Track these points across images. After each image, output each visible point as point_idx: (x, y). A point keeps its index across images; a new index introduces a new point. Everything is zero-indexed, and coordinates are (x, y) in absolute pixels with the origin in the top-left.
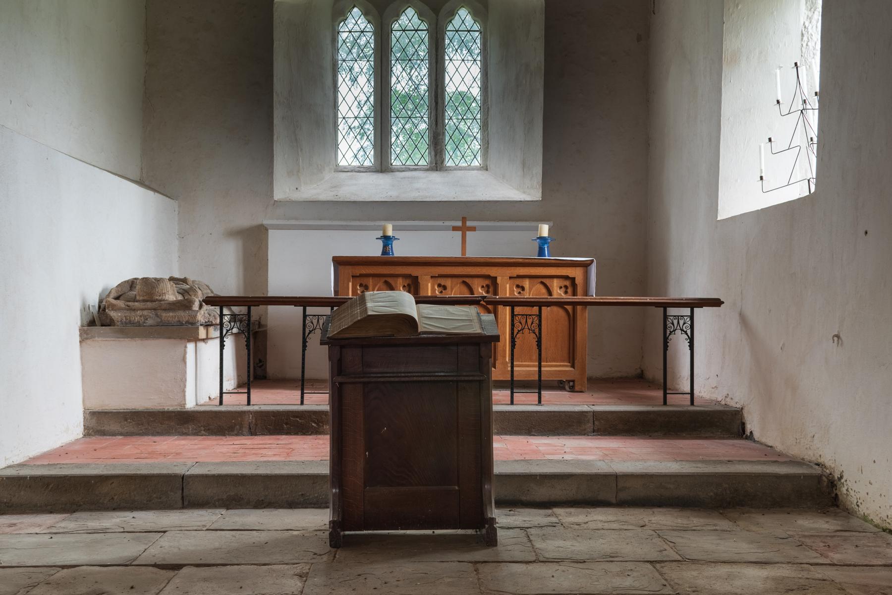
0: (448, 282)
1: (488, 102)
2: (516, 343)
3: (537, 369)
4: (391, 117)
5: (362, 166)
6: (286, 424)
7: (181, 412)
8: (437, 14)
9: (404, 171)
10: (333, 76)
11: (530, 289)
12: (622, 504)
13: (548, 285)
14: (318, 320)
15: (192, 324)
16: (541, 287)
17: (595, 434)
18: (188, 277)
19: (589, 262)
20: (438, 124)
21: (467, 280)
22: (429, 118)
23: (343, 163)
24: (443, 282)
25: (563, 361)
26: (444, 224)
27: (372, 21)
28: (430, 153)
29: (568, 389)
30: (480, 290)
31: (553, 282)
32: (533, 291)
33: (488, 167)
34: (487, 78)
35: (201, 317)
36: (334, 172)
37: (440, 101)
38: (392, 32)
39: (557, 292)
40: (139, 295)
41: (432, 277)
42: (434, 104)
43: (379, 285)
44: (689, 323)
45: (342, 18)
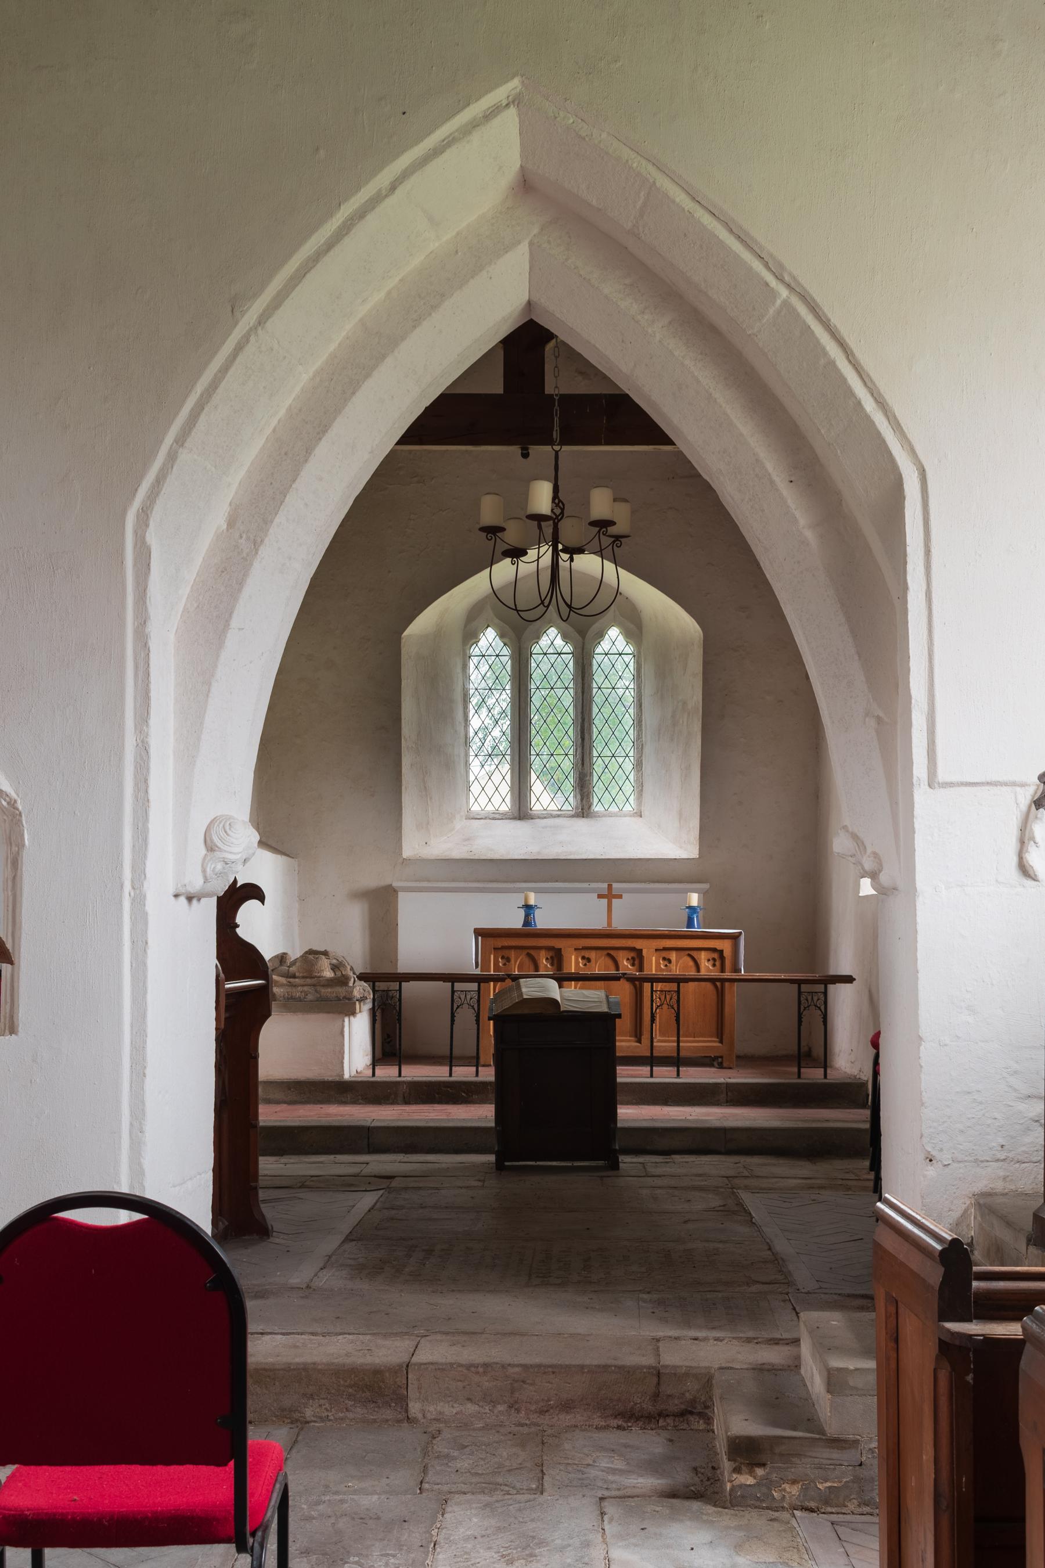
0: (592, 955)
1: (642, 738)
2: (802, 1019)
3: (675, 1044)
4: (530, 755)
5: (497, 812)
6: (438, 1094)
7: (340, 1082)
8: (583, 637)
9: (545, 818)
10: (464, 708)
11: (677, 962)
12: (729, 1152)
13: (695, 957)
14: (466, 996)
15: (349, 999)
16: (689, 959)
17: (728, 1104)
18: (328, 950)
19: (737, 934)
20: (585, 762)
21: (612, 952)
22: (575, 756)
23: (475, 808)
24: (587, 954)
25: (712, 1037)
26: (590, 886)
27: (508, 643)
28: (575, 797)
29: (717, 1066)
30: (625, 963)
31: (701, 954)
32: (680, 966)
33: (642, 813)
34: (641, 710)
35: (357, 993)
36: (466, 819)
37: (586, 736)
38: (531, 656)
39: (705, 965)
40: (299, 971)
41: (575, 949)
42: (580, 740)
43: (521, 958)
44: (823, 999)
45: (474, 641)
